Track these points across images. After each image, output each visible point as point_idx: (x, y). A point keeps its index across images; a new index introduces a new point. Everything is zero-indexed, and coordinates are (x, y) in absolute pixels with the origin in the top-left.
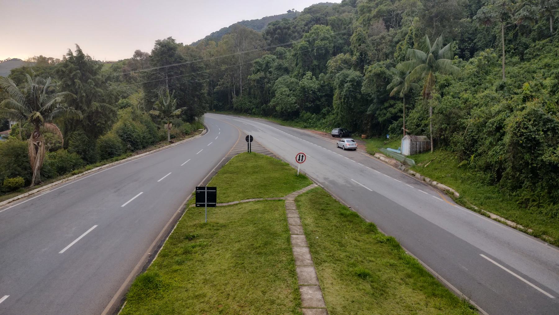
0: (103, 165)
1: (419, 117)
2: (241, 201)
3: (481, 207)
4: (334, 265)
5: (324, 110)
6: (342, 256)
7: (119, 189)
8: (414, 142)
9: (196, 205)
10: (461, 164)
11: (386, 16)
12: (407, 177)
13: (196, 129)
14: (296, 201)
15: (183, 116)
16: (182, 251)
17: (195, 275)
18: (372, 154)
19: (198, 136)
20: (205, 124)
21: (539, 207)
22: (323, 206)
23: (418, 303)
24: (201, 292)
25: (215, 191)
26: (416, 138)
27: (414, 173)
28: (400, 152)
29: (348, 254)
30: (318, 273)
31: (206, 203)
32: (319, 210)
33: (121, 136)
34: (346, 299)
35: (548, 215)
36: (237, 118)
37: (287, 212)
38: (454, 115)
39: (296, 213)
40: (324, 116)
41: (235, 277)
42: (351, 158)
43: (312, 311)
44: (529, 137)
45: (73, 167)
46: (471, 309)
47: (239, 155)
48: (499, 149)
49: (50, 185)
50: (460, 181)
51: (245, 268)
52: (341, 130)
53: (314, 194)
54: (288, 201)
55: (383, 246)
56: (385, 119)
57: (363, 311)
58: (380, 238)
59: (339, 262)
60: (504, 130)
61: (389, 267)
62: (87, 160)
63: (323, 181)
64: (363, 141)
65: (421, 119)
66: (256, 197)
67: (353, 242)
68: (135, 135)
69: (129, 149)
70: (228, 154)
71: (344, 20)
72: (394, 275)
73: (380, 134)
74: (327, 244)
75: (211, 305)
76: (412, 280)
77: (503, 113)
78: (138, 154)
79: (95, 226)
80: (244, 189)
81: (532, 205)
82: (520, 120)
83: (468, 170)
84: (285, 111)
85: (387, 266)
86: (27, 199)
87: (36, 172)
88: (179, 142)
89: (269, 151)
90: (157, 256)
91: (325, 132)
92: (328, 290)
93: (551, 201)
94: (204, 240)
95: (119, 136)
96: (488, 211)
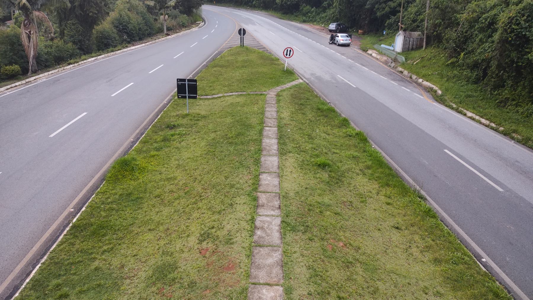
0: (98, 56)
1: (417, 12)
2: (225, 94)
3: (459, 105)
4: (298, 156)
5: (325, 3)
6: (307, 148)
7: (111, 80)
8: (407, 39)
9: (178, 96)
10: (449, 62)
12: (394, 74)
13: (193, 21)
14: (278, 95)
15: (180, 8)
16: (161, 139)
17: (170, 160)
18: (365, 50)
19: (195, 29)
20: (203, 16)
21: (517, 107)
22: (302, 101)
23: (370, 192)
24: (172, 175)
25: (195, 83)
26: (410, 35)
27: (403, 70)
28: (393, 49)
29: (314, 146)
30: (280, 162)
31: (187, 95)
32: (298, 104)
33: (117, 27)
34: (301, 186)
35: (524, 114)
36: (237, 10)
37: (266, 106)
38: (450, 10)
39: (274, 107)
40: (324, 10)
41: (204, 164)
42: (343, 54)
43: (266, 195)
44: (519, 33)
45: (71, 57)
46: (420, 198)
47: (233, 49)
48: (487, 47)
49: (46, 74)
50: (446, 79)
51: (215, 156)
52: (339, 25)
53: (296, 89)
54: (270, 96)
55: (351, 139)
56: (384, 14)
57: (314, 196)
58: (350, 132)
59: (303, 153)
60: (496, 26)
61: (351, 159)
62: (83, 50)
63: (309, 77)
64: (359, 37)
65: (419, 13)
66: (239, 91)
67: (323, 135)
68: (130, 26)
69: (125, 40)
70: (221, 47)
72: (354, 166)
73: (378, 30)
74: (297, 136)
75: (179, 187)
76: (370, 171)
77: (499, 7)
78: (133, 45)
79: (85, 113)
80: (230, 82)
81: (511, 104)
82: (513, 16)
83: (455, 68)
84: (285, 4)
85: (349, 158)
86: (24, 86)
88: (176, 34)
89: (262, 46)
90: (138, 142)
91: (323, 27)
92: (286, 177)
93: (531, 101)
94: (184, 129)
95: (115, 26)
96: (466, 109)
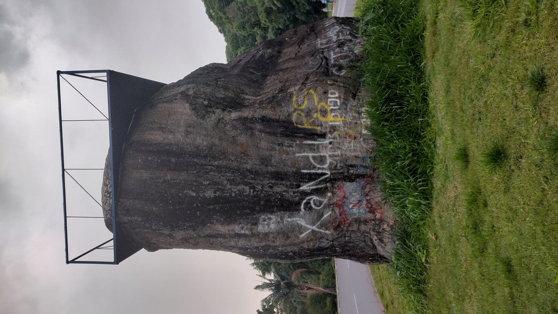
11: (223, 4)
71: (232, 38)
87: (327, 291)
